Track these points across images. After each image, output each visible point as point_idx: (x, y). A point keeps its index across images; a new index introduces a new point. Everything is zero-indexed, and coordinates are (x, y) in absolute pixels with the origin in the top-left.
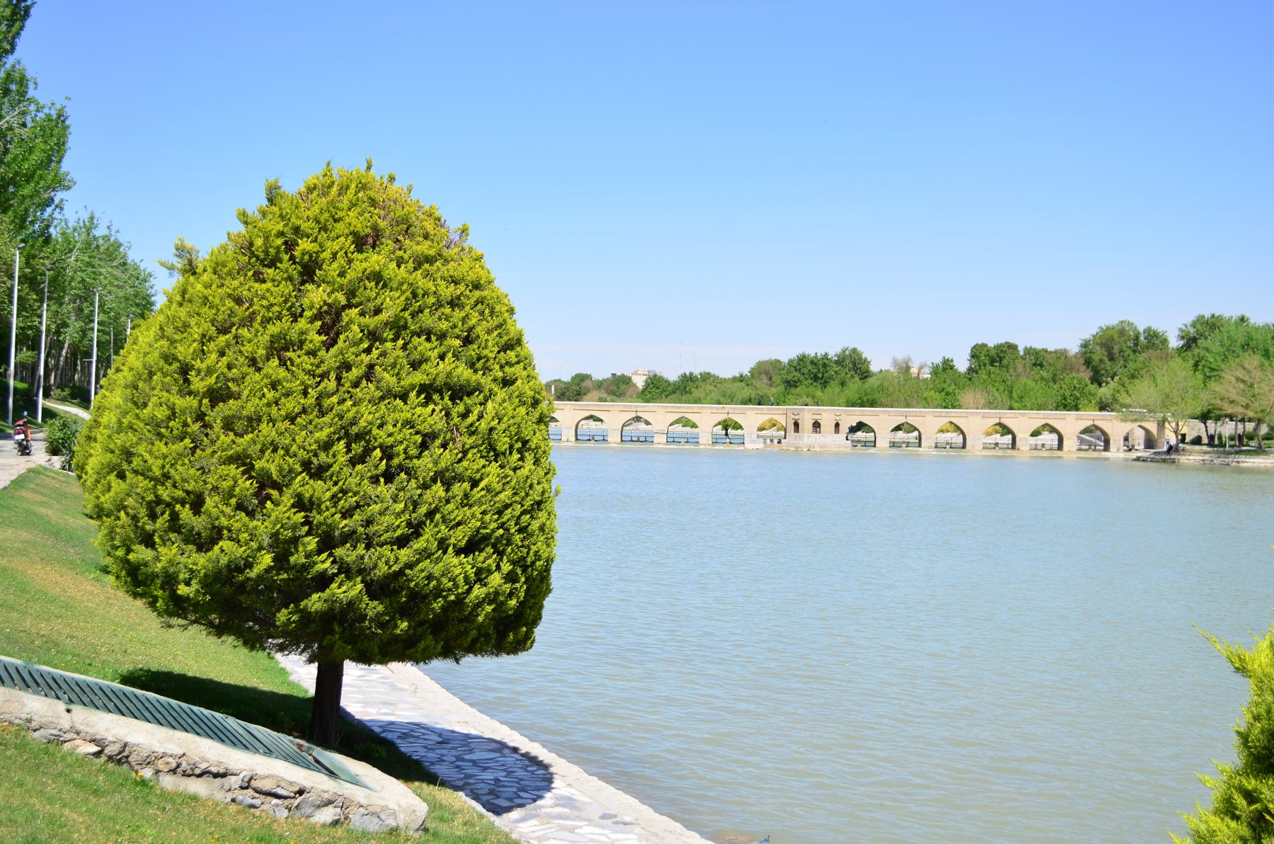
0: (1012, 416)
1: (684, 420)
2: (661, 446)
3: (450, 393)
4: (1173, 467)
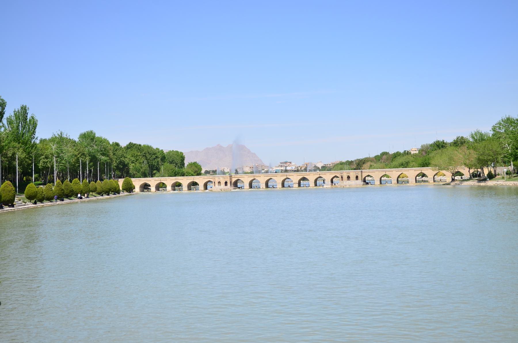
0: (426, 169)
1: (421, 174)
2: (185, 192)
3: (93, 167)
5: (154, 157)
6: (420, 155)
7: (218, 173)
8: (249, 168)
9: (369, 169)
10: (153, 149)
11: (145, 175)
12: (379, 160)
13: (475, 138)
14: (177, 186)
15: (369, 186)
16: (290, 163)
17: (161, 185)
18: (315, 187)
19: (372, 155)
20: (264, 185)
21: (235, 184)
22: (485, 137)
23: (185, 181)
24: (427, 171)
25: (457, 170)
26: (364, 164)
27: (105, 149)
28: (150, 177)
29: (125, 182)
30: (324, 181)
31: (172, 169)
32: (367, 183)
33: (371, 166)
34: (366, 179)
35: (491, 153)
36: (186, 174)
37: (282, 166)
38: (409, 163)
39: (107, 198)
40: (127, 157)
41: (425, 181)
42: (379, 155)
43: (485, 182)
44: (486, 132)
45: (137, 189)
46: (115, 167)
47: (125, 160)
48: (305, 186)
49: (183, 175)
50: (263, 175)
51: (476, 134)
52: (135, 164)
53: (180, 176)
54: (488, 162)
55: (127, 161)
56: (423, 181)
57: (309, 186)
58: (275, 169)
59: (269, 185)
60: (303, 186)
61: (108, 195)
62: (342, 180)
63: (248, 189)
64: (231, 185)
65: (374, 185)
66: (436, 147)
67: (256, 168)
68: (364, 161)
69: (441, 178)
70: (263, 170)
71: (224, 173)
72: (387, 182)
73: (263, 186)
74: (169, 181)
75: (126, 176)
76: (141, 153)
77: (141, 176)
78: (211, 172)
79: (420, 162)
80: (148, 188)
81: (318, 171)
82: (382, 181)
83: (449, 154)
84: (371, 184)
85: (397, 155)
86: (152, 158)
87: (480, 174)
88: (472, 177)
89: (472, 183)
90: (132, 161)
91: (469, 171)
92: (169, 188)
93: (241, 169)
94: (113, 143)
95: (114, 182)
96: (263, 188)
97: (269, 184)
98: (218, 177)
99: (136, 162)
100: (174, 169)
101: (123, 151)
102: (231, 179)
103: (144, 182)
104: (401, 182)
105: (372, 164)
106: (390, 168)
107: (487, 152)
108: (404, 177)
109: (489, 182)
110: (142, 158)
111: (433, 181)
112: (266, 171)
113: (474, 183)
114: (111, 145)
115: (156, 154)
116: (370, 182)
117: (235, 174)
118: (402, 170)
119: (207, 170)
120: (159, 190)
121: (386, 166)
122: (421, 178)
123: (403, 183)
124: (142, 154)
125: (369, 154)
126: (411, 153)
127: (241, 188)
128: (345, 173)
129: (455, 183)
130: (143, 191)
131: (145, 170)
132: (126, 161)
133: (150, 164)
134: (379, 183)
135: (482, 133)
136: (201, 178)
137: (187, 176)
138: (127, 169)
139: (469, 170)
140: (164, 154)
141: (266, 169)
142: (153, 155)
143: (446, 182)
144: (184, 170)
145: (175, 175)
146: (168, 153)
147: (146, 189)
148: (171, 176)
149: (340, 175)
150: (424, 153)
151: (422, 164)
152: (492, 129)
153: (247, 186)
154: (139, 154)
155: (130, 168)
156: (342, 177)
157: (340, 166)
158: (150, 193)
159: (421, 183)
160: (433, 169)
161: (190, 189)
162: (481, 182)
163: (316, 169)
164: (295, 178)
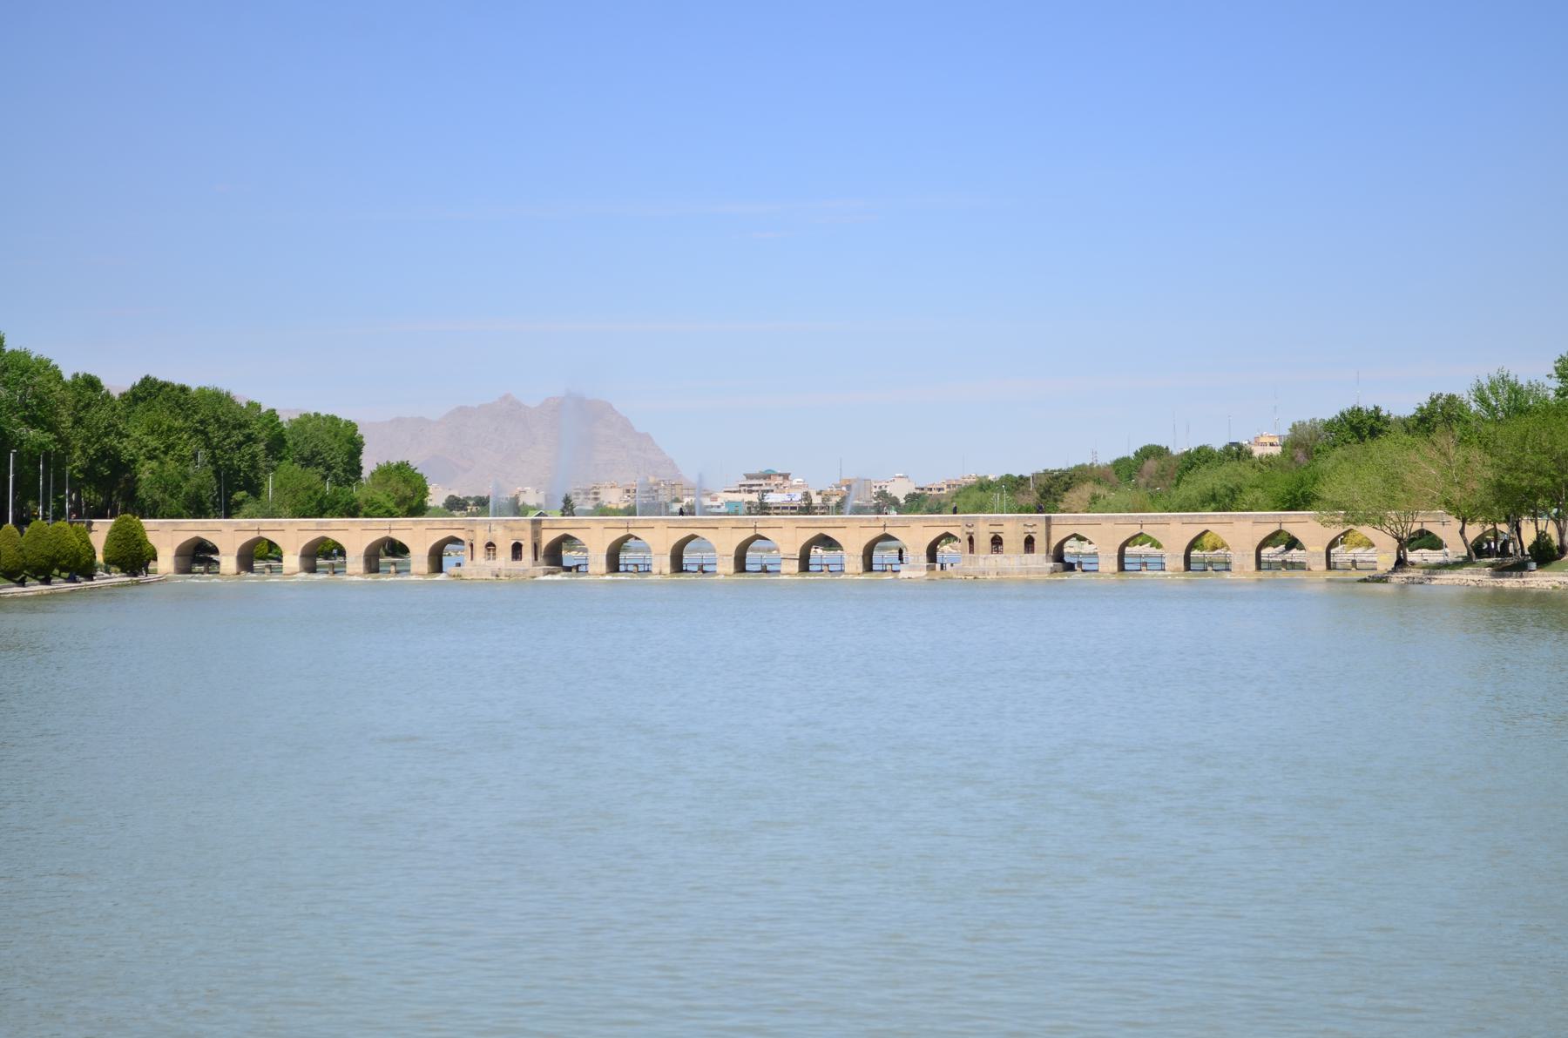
0: (1298, 519)
4: (218, 575)
5: (238, 436)
6: (1286, 462)
7: (495, 510)
8: (620, 491)
9: (1088, 512)
10: (233, 407)
11: (197, 509)
12: (1130, 477)
13: (1489, 405)
14: (321, 554)
15: (1077, 575)
16: (786, 476)
17: (264, 548)
18: (868, 576)
19: (1106, 458)
20: (667, 560)
21: (553, 555)
22: (1531, 402)
23: (356, 535)
24: (1301, 524)
25: (1417, 527)
26: (1066, 490)
27: (42, 402)
28: (220, 517)
29: (117, 534)
30: (901, 552)
31: (309, 488)
32: (1070, 567)
33: (1095, 498)
34: (1065, 550)
35: (1548, 465)
36: (366, 509)
37: (754, 488)
38: (1241, 491)
39: (43, 595)
40: (128, 436)
41: (1293, 566)
42: (1132, 455)
43: (1521, 576)
44: (1533, 383)
45: (165, 563)
46: (80, 471)
47: (121, 446)
48: (889, 567)
49: (352, 511)
50: (664, 524)
51: (1494, 389)
52: (161, 463)
53: (341, 516)
54: (1536, 498)
55: (127, 448)
56: (1284, 563)
57: (842, 571)
58: (723, 497)
59: (685, 561)
60: (819, 568)
61: (47, 581)
62: (971, 550)
63: (602, 575)
64: (536, 559)
65: (1093, 573)
66: (1348, 435)
67: (648, 492)
68: (1067, 479)
69: (1360, 553)
70: (677, 500)
71: (517, 509)
72: (1145, 564)
73: (662, 563)
74: (293, 535)
75: (125, 511)
76: (186, 420)
77: (181, 510)
78: (471, 503)
79: (1281, 489)
80: (212, 561)
81: (893, 514)
82: (1126, 560)
83: (1389, 462)
84: (1084, 571)
85: (1200, 459)
86: (228, 441)
87: (1505, 545)
88: (1474, 554)
89: (1470, 577)
90: (149, 451)
91: (1462, 532)
92: (292, 561)
93: (592, 496)
94: (76, 376)
95: (71, 533)
96: (660, 573)
97: (687, 558)
98: (486, 522)
99: (166, 453)
100: (317, 487)
101: (114, 409)
102: (536, 534)
103: (194, 534)
104: (1201, 566)
105: (1101, 491)
106: (1166, 509)
107: (1530, 458)
108: (1219, 545)
109: (1535, 576)
110: (190, 438)
111: (1324, 567)
112: (688, 506)
113: (1478, 577)
114: (65, 386)
115: (248, 427)
116: (1080, 564)
117: (563, 515)
118: (1204, 520)
119: (457, 495)
120: (250, 569)
121: (1156, 501)
122: (1282, 553)
123: (1210, 568)
124: (189, 424)
125: (1094, 453)
126: (1251, 453)
127: (574, 570)
128: (983, 527)
129: (1406, 575)
130: (189, 571)
131: (200, 487)
132: (125, 448)
133: (220, 463)
134: (1115, 568)
135: (1520, 383)
136: (419, 527)
137: (367, 516)
138: (127, 481)
139: (1463, 528)
140: (279, 425)
141: (686, 500)
142: (234, 428)
143: (1376, 569)
144: (356, 494)
145: (322, 509)
146: (298, 422)
147: (201, 561)
148: (304, 516)
149: (963, 530)
150: (1300, 454)
151: (1288, 497)
152: (1556, 369)
153: (598, 563)
154: (179, 423)
155: (139, 480)
156: (971, 540)
157: (977, 496)
158: (215, 580)
159: (1278, 573)
160: (1325, 518)
161: (373, 567)
162: (1503, 576)
163: (885, 503)
164: (788, 537)
